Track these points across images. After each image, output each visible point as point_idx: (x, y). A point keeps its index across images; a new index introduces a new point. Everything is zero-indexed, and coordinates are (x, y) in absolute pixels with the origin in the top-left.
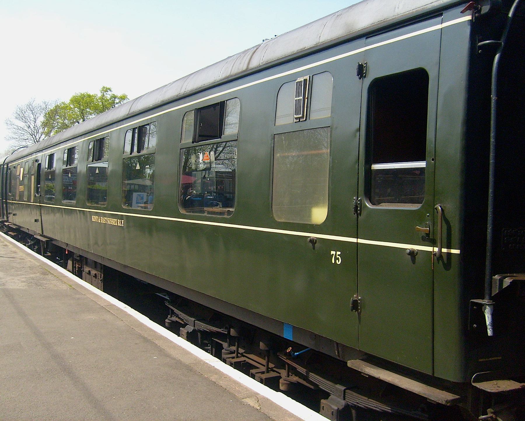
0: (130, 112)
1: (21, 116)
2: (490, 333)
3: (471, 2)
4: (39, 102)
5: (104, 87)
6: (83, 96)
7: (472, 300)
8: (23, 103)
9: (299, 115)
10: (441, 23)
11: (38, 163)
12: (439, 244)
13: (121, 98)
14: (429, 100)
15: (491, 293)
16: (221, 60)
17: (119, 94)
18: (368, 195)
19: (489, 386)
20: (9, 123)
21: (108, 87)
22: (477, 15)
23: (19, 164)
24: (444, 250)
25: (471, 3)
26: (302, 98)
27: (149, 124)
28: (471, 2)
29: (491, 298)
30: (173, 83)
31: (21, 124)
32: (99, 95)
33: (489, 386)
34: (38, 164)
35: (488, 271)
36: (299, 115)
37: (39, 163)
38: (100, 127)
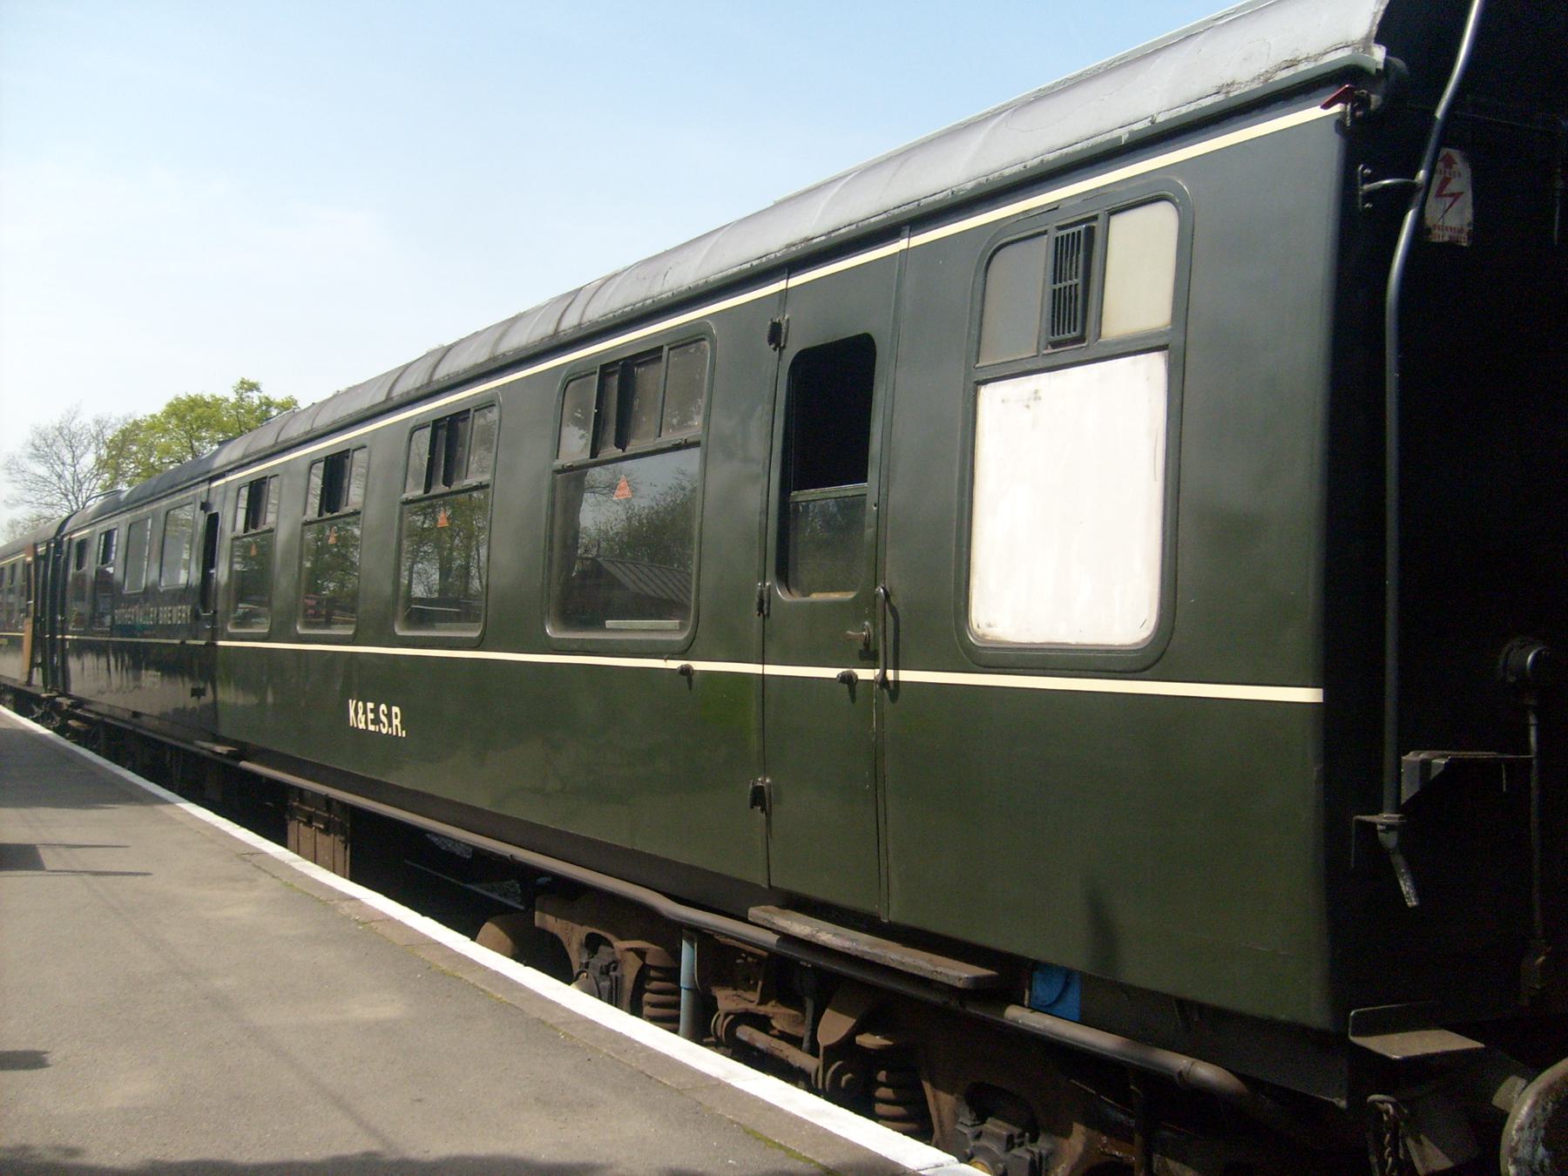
0: (279, 440)
1: (43, 449)
2: (1412, 902)
3: (1347, 86)
4: (85, 420)
5: (242, 382)
6: (195, 403)
7: (1359, 817)
8: (50, 418)
9: (1062, 336)
10: (211, 492)
11: (209, 513)
12: (881, 663)
13: (282, 407)
14: (1000, 373)
15: (1399, 797)
16: (764, 208)
17: (278, 396)
18: (784, 574)
19: (1398, 1046)
20: (12, 467)
21: (253, 380)
22: (1359, 113)
23: (1045, 233)
24: (890, 674)
25: (1347, 88)
26: (1078, 281)
27: (662, 347)
28: (1347, 86)
29: (1398, 808)
30: (736, 225)
31: (42, 470)
32: (233, 398)
33: (1398, 1046)
34: (210, 516)
35: (1390, 737)
36: (1056, 336)
37: (214, 511)
38: (285, 445)
